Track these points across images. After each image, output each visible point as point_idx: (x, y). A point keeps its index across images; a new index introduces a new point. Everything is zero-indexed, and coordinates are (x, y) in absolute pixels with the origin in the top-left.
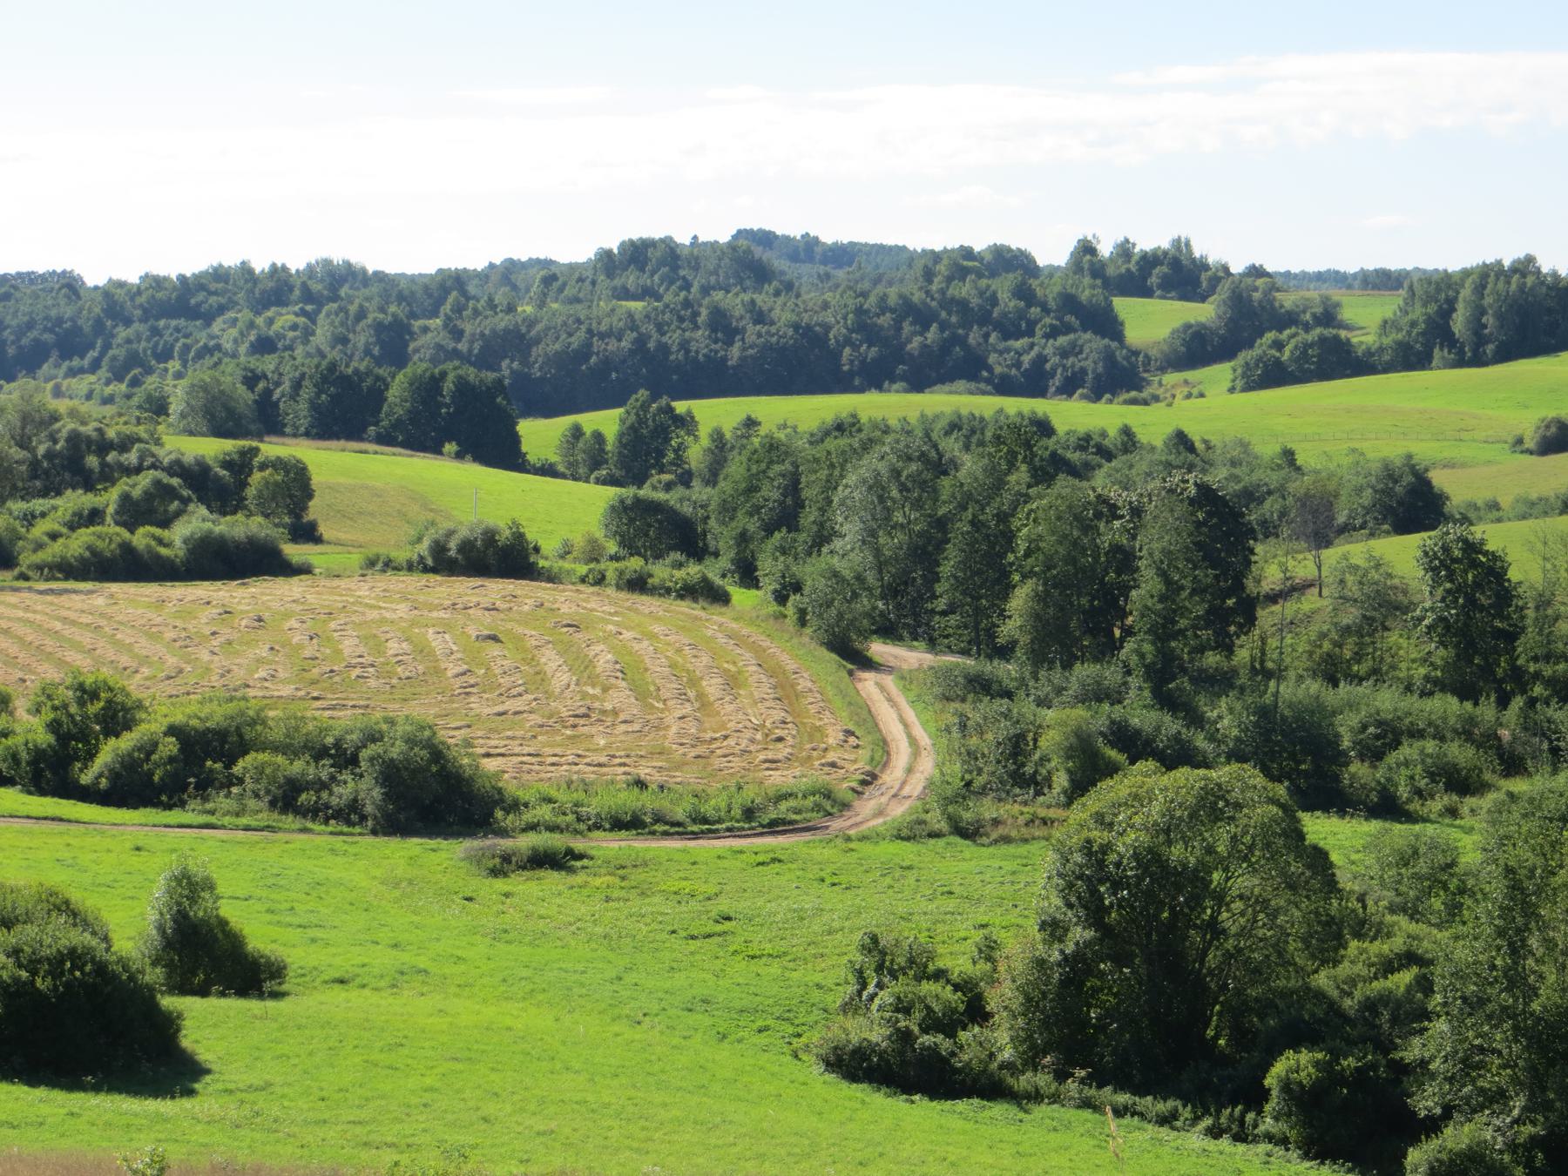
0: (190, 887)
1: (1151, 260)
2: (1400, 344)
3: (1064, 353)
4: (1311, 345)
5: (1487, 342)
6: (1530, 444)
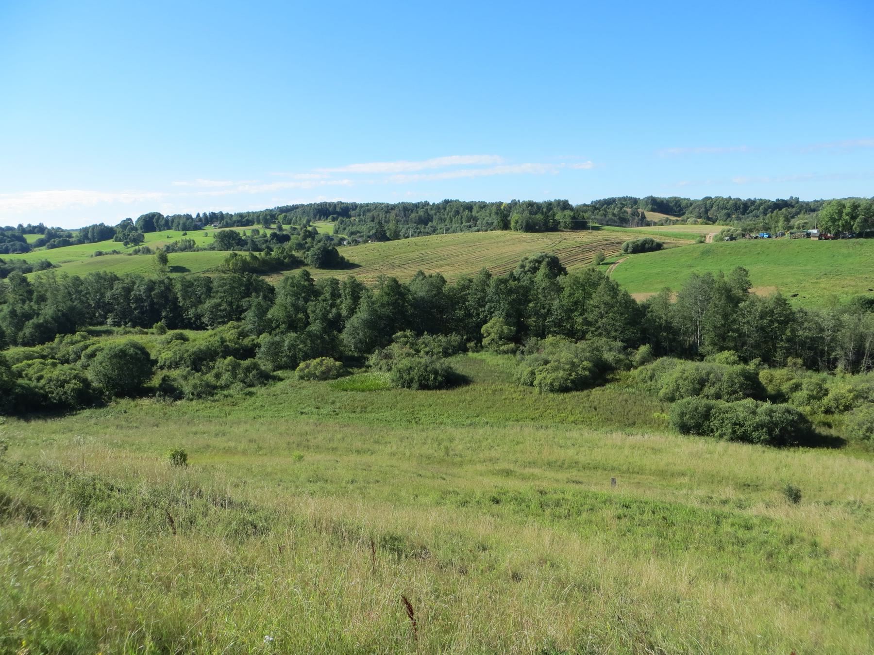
1: (35, 227)
3: (12, 245)
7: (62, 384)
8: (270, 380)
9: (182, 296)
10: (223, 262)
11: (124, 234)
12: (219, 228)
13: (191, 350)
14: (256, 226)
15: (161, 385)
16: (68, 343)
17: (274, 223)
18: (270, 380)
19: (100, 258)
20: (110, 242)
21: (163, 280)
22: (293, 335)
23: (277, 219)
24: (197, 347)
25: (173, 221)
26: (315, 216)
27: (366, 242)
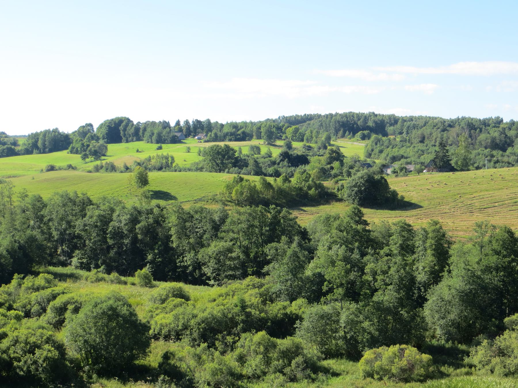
2: (26, 149)
4: (5, 149)
5: (46, 148)
6: (44, 171)
7: (32, 349)
8: (320, 374)
9: (177, 232)
10: (222, 189)
11: (83, 144)
12: (205, 142)
13: (201, 315)
14: (255, 142)
15: (160, 365)
16: (29, 288)
17: (280, 138)
18: (320, 374)
19: (52, 174)
20: (64, 153)
21: (152, 210)
22: (353, 306)
23: (285, 133)
24: (208, 311)
25: (145, 130)
26: (337, 131)
27: (420, 171)
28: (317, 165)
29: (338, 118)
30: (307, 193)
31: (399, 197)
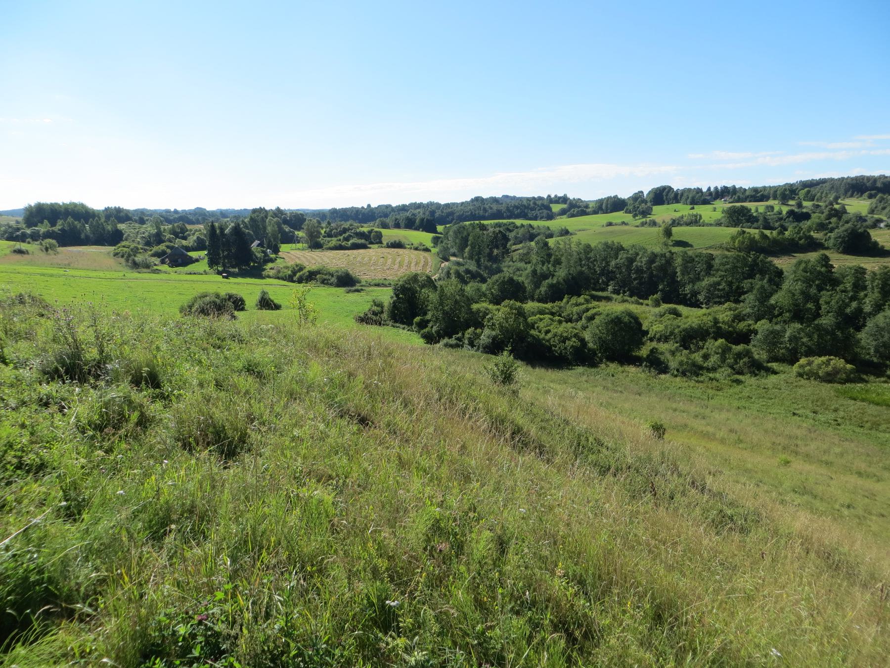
0: (264, 293)
1: (560, 198)
9: (681, 270)
10: (728, 239)
12: (730, 203)
14: (771, 202)
15: (648, 356)
17: (793, 199)
19: (610, 228)
21: (665, 254)
25: (682, 195)
28: (817, 221)
29: (849, 181)
30: (798, 243)
31: (880, 246)
